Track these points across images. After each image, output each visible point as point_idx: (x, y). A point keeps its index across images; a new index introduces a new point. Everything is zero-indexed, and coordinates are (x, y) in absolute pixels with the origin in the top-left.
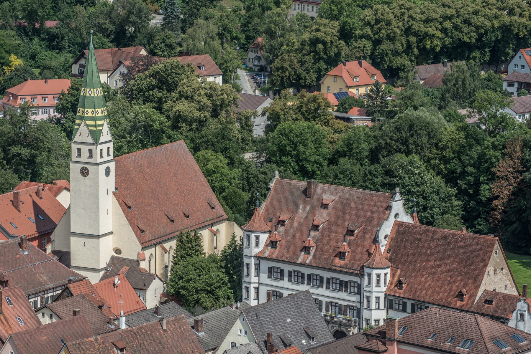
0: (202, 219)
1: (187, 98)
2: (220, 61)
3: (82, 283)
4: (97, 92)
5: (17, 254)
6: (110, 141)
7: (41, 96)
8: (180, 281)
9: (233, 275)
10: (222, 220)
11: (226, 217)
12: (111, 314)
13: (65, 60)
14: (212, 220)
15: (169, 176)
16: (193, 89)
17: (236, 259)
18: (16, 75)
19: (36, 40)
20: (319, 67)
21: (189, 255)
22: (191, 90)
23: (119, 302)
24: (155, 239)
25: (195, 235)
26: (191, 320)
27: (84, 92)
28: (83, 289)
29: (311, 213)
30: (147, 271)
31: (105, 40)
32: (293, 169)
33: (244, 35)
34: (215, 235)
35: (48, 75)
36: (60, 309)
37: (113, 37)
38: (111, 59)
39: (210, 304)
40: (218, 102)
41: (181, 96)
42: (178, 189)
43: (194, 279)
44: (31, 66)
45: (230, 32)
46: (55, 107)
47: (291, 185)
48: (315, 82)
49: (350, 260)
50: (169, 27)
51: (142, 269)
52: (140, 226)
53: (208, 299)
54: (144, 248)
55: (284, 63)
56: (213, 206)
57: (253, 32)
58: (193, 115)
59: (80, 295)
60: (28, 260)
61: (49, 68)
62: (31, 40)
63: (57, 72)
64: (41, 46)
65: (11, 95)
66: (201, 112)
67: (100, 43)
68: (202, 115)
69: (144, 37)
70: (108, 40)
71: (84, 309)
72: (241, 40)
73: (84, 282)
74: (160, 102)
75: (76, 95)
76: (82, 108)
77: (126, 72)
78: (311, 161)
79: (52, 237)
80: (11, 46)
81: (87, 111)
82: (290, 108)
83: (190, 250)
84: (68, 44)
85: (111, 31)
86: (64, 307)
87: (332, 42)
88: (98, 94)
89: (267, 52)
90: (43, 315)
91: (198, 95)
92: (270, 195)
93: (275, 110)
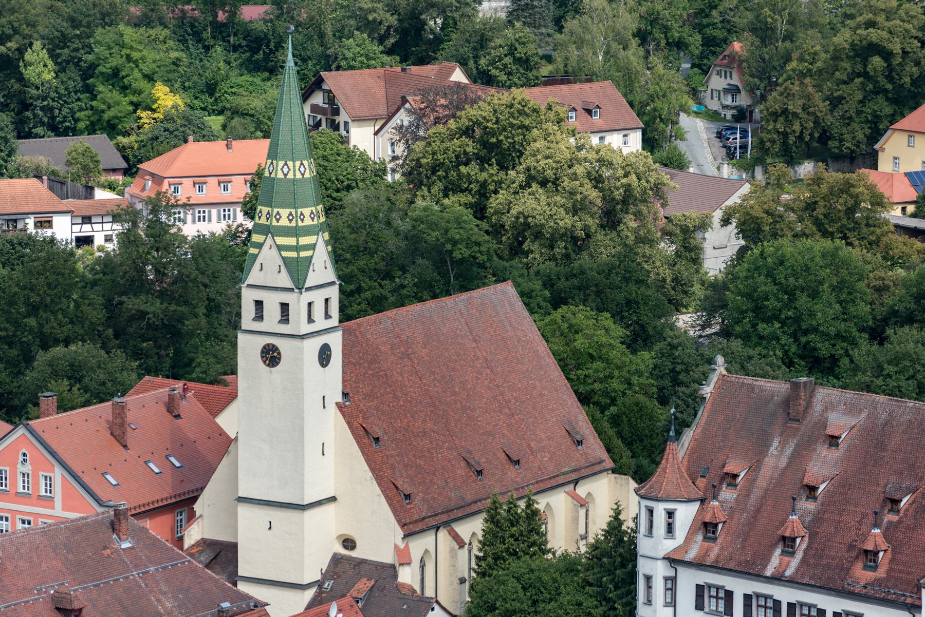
0: (551, 468)
1: (543, 183)
2: (639, 96)
4: (302, 169)
5: (105, 548)
6: (332, 284)
7: (216, 178)
9: (615, 602)
11: (609, 464)
14: (572, 471)
15: (473, 367)
16: (558, 162)
17: (623, 566)
18: (166, 130)
19: (219, 49)
20: (875, 111)
21: (515, 553)
24: (436, 515)
25: (529, 506)
27: (271, 168)
29: (799, 457)
30: (414, 591)
32: (786, 353)
33: (698, 37)
35: (242, 131)
37: (392, 40)
38: (383, 92)
40: (616, 193)
42: (495, 398)
45: (666, 29)
46: (241, 205)
47: (753, 389)
48: (864, 147)
49: (889, 572)
50: (525, 17)
51: (403, 585)
52: (399, 483)
55: (791, 103)
56: (579, 438)
57: (723, 28)
60: (131, 562)
61: (244, 115)
62: (207, 48)
63: (261, 122)
64: (229, 64)
65: (147, 177)
66: (576, 218)
67: (362, 55)
70: (381, 48)
72: (692, 48)
74: (484, 193)
78: (827, 334)
79: (198, 507)
80: (159, 63)
81: (278, 213)
82: (789, 208)
85: (389, 27)
87: (905, 53)
88: (303, 175)
89: (752, 76)
91: (570, 179)
92: (703, 414)
93: (753, 212)
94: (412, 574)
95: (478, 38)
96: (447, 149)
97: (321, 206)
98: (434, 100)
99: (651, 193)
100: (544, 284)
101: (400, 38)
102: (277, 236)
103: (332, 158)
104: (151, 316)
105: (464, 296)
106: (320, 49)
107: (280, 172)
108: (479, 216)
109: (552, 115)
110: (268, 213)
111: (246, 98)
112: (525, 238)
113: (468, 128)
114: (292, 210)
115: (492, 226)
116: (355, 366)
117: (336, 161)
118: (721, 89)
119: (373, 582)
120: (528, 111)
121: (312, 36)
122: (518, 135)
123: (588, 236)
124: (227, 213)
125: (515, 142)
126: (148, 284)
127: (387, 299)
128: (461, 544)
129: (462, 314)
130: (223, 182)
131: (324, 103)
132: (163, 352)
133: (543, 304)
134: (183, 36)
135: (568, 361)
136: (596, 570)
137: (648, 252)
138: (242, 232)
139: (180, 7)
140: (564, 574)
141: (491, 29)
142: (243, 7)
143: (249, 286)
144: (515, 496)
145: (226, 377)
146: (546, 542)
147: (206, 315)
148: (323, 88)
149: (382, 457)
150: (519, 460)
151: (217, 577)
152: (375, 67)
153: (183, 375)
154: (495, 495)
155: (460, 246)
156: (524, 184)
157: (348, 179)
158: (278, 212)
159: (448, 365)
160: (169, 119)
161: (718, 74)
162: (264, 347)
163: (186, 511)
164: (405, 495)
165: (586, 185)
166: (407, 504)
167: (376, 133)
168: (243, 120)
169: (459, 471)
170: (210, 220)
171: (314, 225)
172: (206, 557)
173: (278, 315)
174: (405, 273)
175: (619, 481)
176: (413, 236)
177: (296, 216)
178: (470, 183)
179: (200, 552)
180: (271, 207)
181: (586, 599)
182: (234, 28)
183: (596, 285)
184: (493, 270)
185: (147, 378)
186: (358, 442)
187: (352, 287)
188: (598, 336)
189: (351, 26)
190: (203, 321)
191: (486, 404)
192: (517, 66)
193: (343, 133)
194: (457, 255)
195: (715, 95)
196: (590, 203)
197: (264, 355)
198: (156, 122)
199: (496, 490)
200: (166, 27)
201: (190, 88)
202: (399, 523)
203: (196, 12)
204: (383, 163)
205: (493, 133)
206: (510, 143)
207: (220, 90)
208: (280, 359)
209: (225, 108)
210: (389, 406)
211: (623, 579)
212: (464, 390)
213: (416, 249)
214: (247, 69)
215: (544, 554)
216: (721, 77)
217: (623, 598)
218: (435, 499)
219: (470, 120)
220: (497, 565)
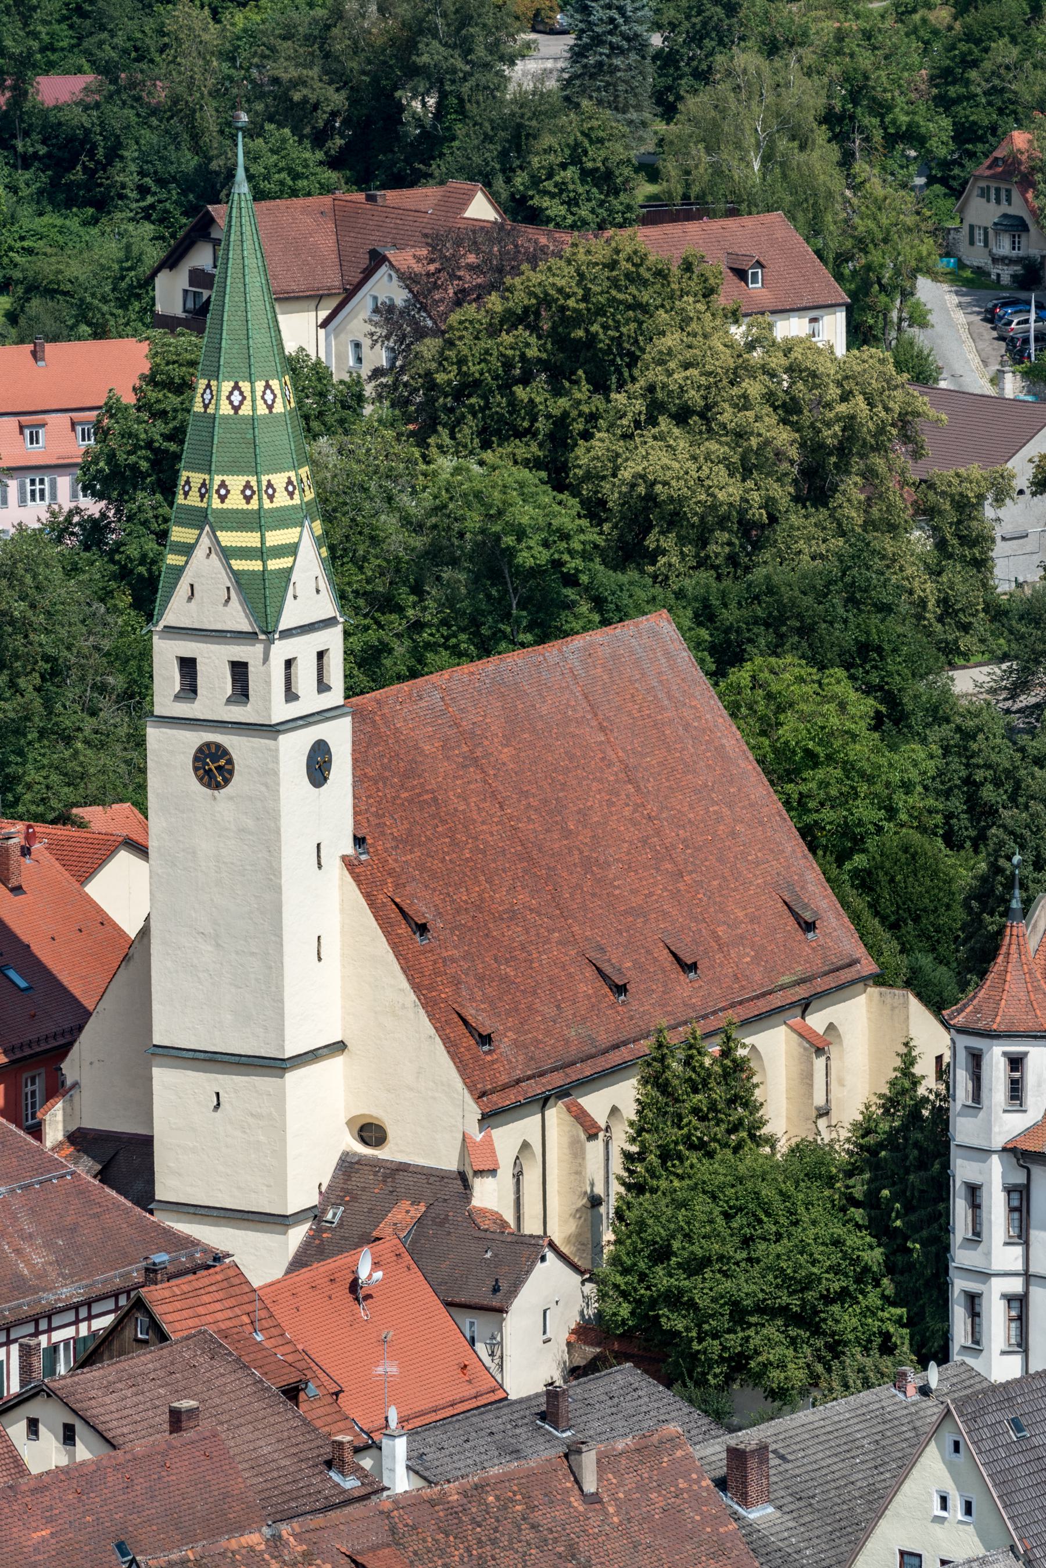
0: (758, 977)
1: (682, 417)
2: (834, 242)
3: (206, 1281)
4: (269, 397)
6: (328, 623)
8: (660, 1270)
10: (853, 982)
11: (868, 966)
13: (121, 255)
15: (600, 781)
16: (709, 374)
17: (922, 1165)
22: (703, 380)
23: (380, 1370)
24: (542, 1074)
25: (726, 1053)
26: (709, 1451)
27: (207, 396)
30: (504, 1224)
31: (307, 155)
33: (946, 122)
34: (819, 1051)
35: (50, 325)
36: (107, 1400)
37: (339, 142)
39: (802, 1374)
40: (827, 433)
41: (655, 409)
42: (645, 841)
43: (721, 1258)
45: (881, 109)
50: (598, 89)
51: (483, 1212)
52: (469, 1013)
53: (790, 1353)
54: (489, 1118)
56: (808, 916)
57: (990, 104)
58: (713, 495)
61: (51, 292)
63: (90, 307)
64: (16, 193)
66: (750, 484)
68: (755, 497)
70: (320, 155)
71: (218, 1401)
73: (216, 1275)
75: (175, 410)
77: (399, 302)
79: (70, 1069)
81: (223, 485)
84: (136, 178)
85: (334, 114)
86: (129, 1393)
88: (270, 407)
90: (33, 1426)
91: (735, 406)
96: (487, 352)
97: (307, 468)
99: (895, 431)
102: (222, 529)
106: (195, 161)
110: (204, 485)
111: (53, 259)
113: (526, 309)
114: (250, 478)
116: (376, 783)
118: (990, 225)
120: (647, 275)
122: (628, 321)
123: (773, 519)
125: (622, 334)
129: (575, 677)
137: (890, 550)
142: (39, 79)
149: (435, 962)
150: (695, 964)
155: (532, 543)
158: (223, 482)
159: (553, 779)
161: (982, 196)
162: (200, 750)
163: (43, 1075)
165: (767, 419)
166: (486, 1053)
169: (582, 987)
171: (294, 507)
174: (422, 600)
175: (889, 1000)
180: (209, 472)
186: (387, 934)
188: (823, 716)
191: (628, 853)
192: (587, 187)
194: (525, 558)
195: (977, 237)
197: (199, 764)
202: (471, 1092)
205: (579, 320)
206: (612, 339)
210: (443, 860)
211: (922, 1191)
212: (585, 827)
214: (51, 201)
215: (758, 1145)
216: (988, 201)
217: (922, 1229)
219: (531, 294)
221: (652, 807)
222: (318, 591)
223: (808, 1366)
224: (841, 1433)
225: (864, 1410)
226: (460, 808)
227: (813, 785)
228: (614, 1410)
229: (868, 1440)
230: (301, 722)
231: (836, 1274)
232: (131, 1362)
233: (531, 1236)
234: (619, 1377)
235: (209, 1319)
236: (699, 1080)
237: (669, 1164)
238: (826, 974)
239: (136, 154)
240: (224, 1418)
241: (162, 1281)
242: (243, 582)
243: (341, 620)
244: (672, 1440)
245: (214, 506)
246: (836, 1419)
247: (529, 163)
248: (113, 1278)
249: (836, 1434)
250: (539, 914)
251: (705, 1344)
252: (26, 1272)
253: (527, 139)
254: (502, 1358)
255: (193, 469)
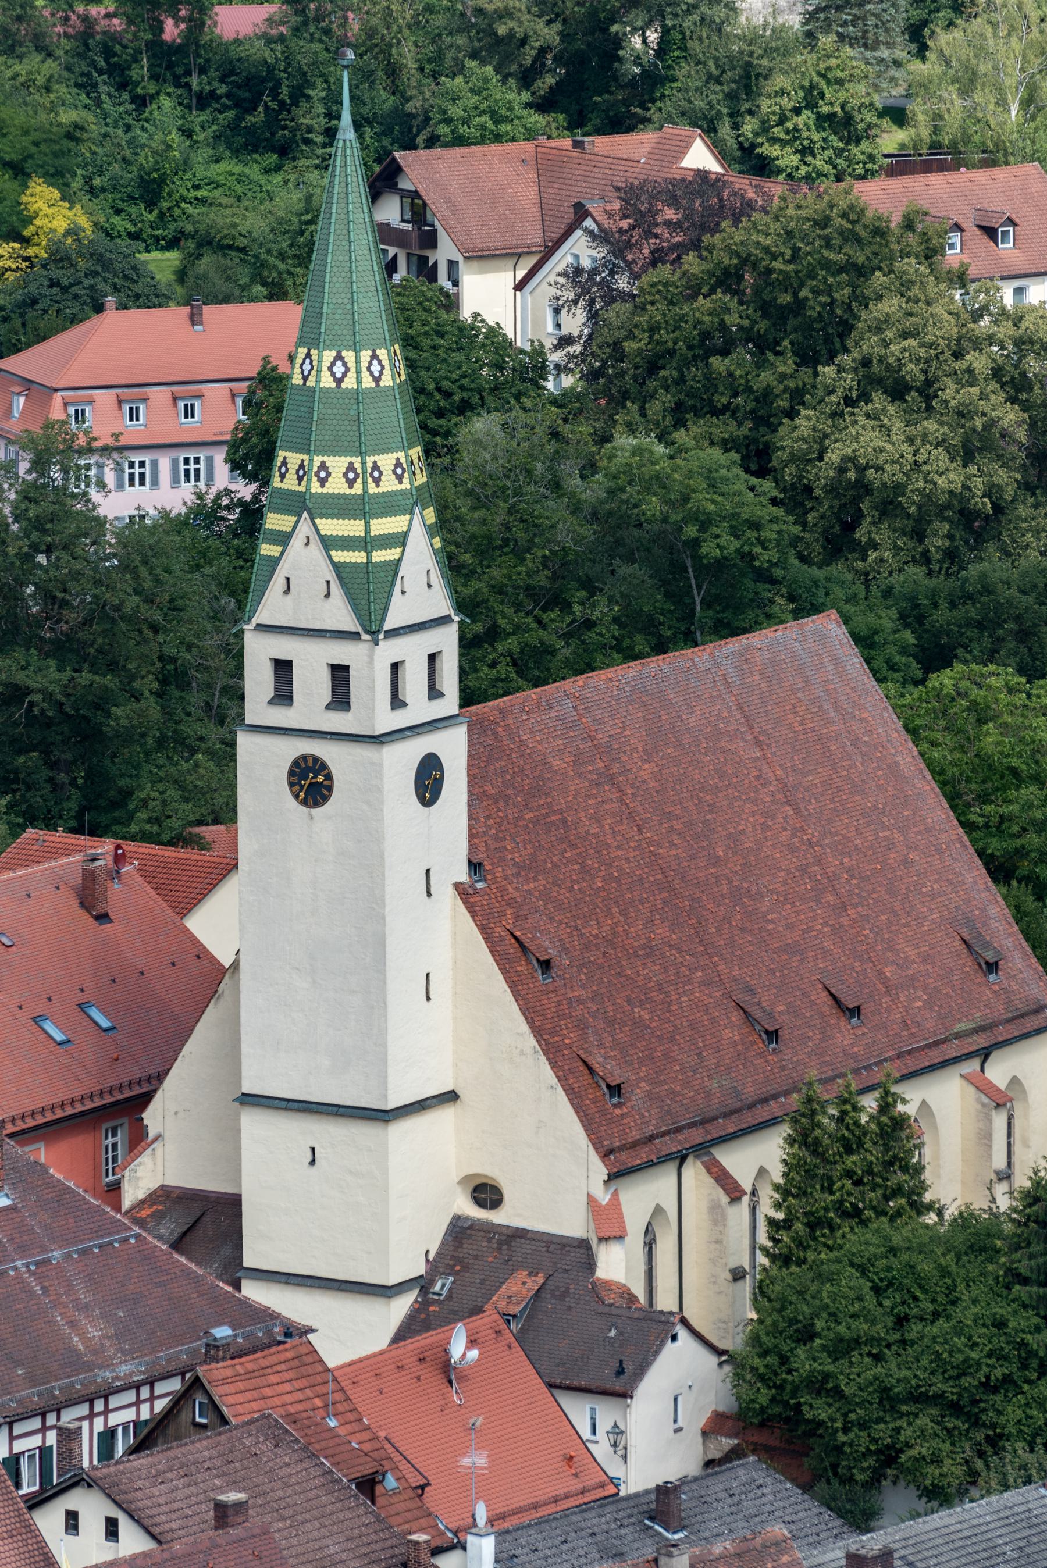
0: (930, 1024)
1: (898, 391)
3: (274, 1359)
4: (376, 368)
6: (442, 621)
8: (801, 1352)
12: (423, 1522)
14: (977, 1031)
15: (755, 802)
16: (930, 346)
19: (166, 102)
21: (856, 1213)
22: (922, 352)
23: (466, 1461)
24: (678, 1130)
25: (885, 1107)
26: (830, 1556)
27: (307, 367)
28: (280, 1389)
30: (632, 1298)
31: (511, 96)
35: (220, 284)
37: (550, 80)
38: (532, 193)
39: (959, 1471)
42: (803, 870)
43: (872, 1340)
44: (134, 236)
50: (845, 24)
51: (608, 1284)
52: (596, 1060)
53: (947, 1446)
56: (990, 956)
59: (264, 1423)
60: (11, 1240)
61: (224, 248)
62: (141, 102)
63: (264, 264)
65: (16, 389)
66: (972, 469)
68: (978, 484)
69: (710, 77)
70: (526, 96)
71: (280, 1493)
73: (289, 1350)
76: (299, 450)
77: (586, 263)
79: (152, 1117)
80: (35, 136)
81: (323, 466)
83: (856, 1190)
84: (323, 120)
85: (543, 51)
86: (180, 1483)
88: (377, 380)
90: (72, 1521)
91: (958, 382)
94: (627, 1261)
95: (739, 71)
96: (682, 318)
98: (649, 211)
100: (903, 616)
101: (567, 73)
103: (425, 343)
104: (37, 697)
105: (734, 645)
107: (325, 374)
108: (754, 467)
109: (912, 240)
110: (302, 466)
111: (228, 211)
112: (859, 516)
114: (354, 459)
115: (784, 490)
116: (496, 802)
117: (434, 347)
119: (540, 1280)
120: (863, 234)
121: (372, 73)
124: (192, 467)
126: (30, 626)
127: (552, 652)
128: (735, 1193)
130: (182, 398)
131: (403, 221)
132: (63, 777)
133: (899, 659)
134: (88, 75)
135: (962, 786)
136: (1035, 1248)
138: (227, 508)
139: (80, 9)
140: (965, 1258)
141: (768, 51)
143: (261, 628)
144: (854, 1087)
145: (197, 830)
146: (923, 1187)
147: (159, 695)
148: (401, 186)
149: (559, 1003)
150: (858, 1008)
151: (200, 1272)
152: (513, 140)
153: (108, 826)
154: (810, 1084)
155: (716, 531)
156: (854, 394)
157: (462, 388)
158: (323, 463)
159: (699, 799)
160: (61, 260)
162: (296, 763)
163: (126, 1126)
164: (608, 1086)
165: (993, 397)
166: (615, 1106)
167: (519, 286)
168: (222, 261)
169: (727, 1033)
170: (155, 483)
171: (402, 492)
172: (170, 1228)
173: (324, 690)
176: (610, 513)
177: (364, 472)
178: (735, 395)
179: (158, 1217)
181: (1015, 1312)
182: (199, 56)
183: (1018, 619)
184: (789, 587)
185: (30, 832)
186: (504, 971)
187: (479, 628)
189: (459, 49)
190: (152, 708)
191: (784, 883)
192: (824, 135)
193: (444, 282)
194: (709, 549)
196: (1003, 436)
197: (295, 779)
198: (32, 267)
199: (813, 1074)
200: (50, 55)
201: (103, 190)
202: (596, 1148)
203: (116, 21)
204: (539, 352)
205: (785, 283)
206: (824, 305)
207: (170, 194)
208: (330, 789)
209: (182, 232)
210: (571, 889)
212: (735, 853)
213: (619, 542)
215: (919, 1213)
218: (673, 1092)
220: (815, 1239)
221: (813, 832)
222: (429, 586)
223: (967, 1462)
224: (980, 1538)
225: (1008, 1513)
226: (593, 831)
227: (1014, 808)
228: (733, 1509)
229: (1012, 1546)
230: (408, 733)
231: (998, 1359)
232: (183, 1450)
233: (662, 1312)
234: (741, 1472)
235: (277, 1401)
236: (854, 1140)
237: (818, 1233)
238: (1009, 1021)
239: (324, 94)
240: (287, 1513)
241: (224, 1359)
242: (344, 575)
243: (456, 619)
244: (777, 1544)
245: (313, 491)
246: (975, 1522)
247: (758, 106)
248: (181, 1353)
249: (974, 1540)
250: (680, 951)
251: (852, 1435)
252: (81, 1347)
253: (757, 79)
254: (626, 1448)
255: (290, 449)
